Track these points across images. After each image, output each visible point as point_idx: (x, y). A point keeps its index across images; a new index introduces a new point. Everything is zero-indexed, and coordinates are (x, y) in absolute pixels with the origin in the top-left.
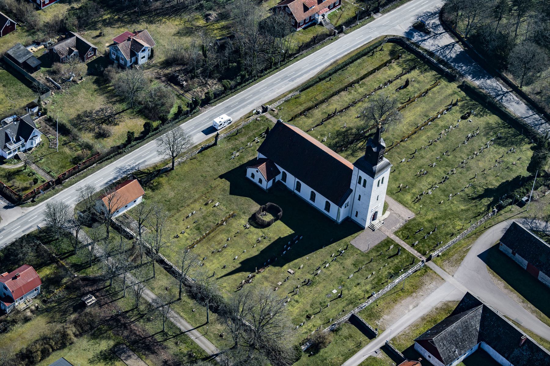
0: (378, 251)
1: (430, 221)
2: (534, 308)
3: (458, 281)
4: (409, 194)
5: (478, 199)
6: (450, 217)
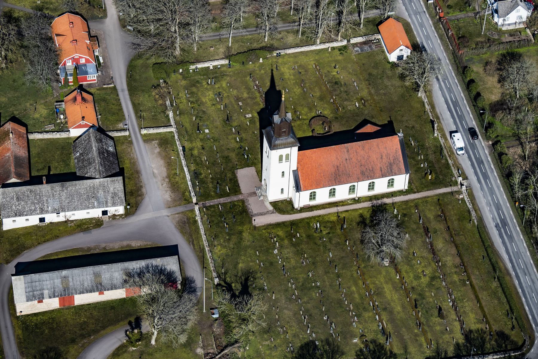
0: (231, 180)
1: (241, 232)
2: (92, 252)
3: (159, 217)
4: (285, 236)
5: (243, 282)
6: (236, 250)
